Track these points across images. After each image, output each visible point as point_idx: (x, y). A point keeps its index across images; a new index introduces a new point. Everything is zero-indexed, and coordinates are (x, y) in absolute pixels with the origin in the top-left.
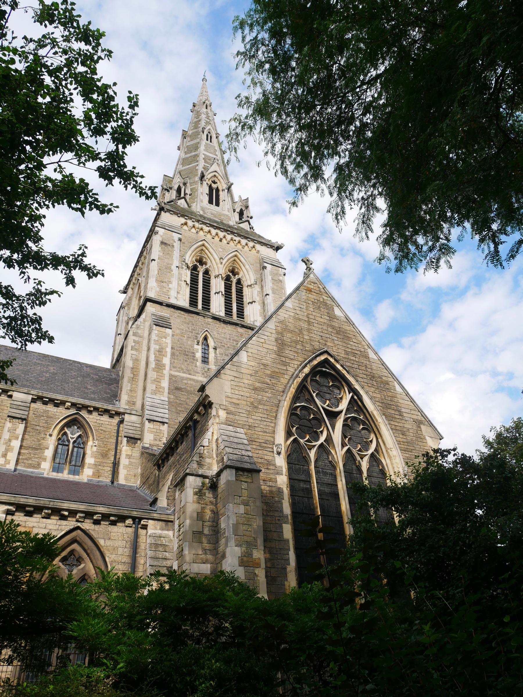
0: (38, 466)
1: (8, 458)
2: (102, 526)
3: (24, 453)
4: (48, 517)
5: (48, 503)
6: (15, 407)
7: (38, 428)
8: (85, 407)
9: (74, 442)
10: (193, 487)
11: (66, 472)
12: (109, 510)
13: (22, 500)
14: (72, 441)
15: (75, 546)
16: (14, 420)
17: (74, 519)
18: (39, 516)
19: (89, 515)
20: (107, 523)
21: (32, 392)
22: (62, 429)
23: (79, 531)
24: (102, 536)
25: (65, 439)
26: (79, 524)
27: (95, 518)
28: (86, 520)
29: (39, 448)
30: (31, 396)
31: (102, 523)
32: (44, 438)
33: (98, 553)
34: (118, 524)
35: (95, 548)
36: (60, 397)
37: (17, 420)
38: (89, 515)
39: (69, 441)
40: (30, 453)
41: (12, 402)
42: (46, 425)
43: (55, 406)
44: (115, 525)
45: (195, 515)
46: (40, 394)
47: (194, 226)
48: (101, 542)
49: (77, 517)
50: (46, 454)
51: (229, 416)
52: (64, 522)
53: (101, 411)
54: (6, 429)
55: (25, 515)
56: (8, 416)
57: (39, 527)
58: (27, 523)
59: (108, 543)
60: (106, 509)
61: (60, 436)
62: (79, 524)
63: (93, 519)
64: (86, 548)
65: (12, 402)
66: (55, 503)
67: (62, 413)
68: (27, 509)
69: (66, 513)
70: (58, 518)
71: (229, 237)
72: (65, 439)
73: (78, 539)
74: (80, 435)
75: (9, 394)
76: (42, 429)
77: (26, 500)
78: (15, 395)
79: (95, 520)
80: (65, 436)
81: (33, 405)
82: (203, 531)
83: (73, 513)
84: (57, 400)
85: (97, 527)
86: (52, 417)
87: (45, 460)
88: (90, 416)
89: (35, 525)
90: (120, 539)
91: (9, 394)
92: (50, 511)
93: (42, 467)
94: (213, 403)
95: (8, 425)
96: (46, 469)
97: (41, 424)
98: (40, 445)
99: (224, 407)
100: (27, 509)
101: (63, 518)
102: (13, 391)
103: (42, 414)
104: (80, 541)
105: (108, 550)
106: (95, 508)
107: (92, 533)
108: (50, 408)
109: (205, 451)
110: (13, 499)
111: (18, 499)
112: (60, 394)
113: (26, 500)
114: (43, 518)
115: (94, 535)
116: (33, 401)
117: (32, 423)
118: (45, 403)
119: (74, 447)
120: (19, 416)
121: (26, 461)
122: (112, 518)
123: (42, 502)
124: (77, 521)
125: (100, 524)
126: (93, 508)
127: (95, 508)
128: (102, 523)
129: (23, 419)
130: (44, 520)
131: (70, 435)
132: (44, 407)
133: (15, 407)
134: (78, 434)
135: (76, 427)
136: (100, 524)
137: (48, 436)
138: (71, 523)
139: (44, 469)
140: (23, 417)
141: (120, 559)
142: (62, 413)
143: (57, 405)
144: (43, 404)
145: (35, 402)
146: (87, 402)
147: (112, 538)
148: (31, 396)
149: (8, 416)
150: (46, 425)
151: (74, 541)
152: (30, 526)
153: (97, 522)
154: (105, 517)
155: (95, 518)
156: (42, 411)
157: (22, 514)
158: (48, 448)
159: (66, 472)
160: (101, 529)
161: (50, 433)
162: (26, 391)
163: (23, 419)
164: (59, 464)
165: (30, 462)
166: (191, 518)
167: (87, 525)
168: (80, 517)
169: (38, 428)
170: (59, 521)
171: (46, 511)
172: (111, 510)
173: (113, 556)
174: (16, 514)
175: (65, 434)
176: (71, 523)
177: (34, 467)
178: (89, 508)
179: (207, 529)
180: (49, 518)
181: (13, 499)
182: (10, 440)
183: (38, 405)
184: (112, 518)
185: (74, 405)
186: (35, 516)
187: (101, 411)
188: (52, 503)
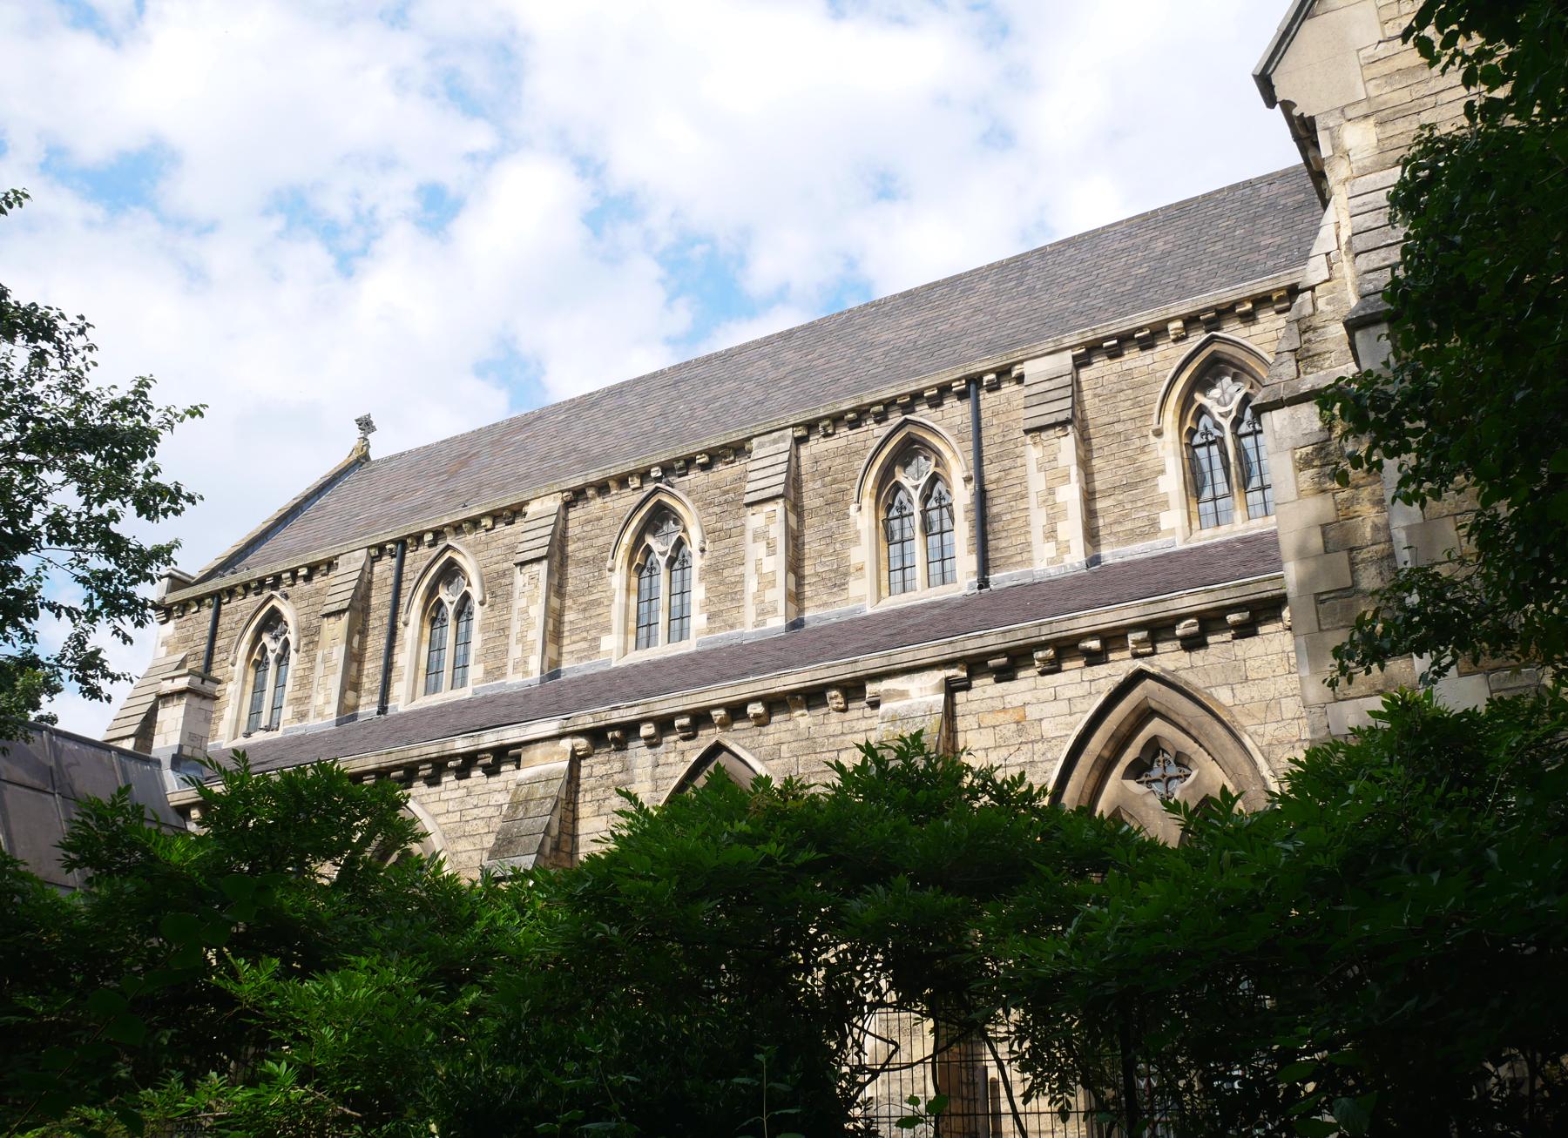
0: (1153, 527)
1: (1061, 536)
2: (1211, 649)
3: (1105, 510)
4: (1053, 667)
5: (1035, 632)
6: (1035, 400)
7: (1118, 427)
8: (1224, 313)
9: (1237, 422)
10: (1288, 444)
11: (1239, 515)
12: (1212, 597)
13: (971, 645)
14: (1226, 424)
15: (1155, 727)
16: (1044, 435)
17: (1127, 654)
18: (1032, 672)
19: (1158, 630)
20: (1228, 636)
21: (1067, 342)
22: (1187, 401)
23: (1148, 682)
24: (1220, 679)
25: (1210, 426)
26: (1140, 664)
27: (1178, 632)
28: (1160, 647)
29: (1140, 480)
30: (1069, 354)
31: (1210, 639)
32: (1142, 449)
33: (1219, 728)
34: (1261, 630)
35: (1208, 718)
36: (1144, 318)
37: (1051, 432)
38: (1158, 630)
39: (1218, 426)
40: (1121, 503)
41: (1027, 392)
42: (1135, 412)
43: (1143, 349)
44: (1255, 634)
45: (1316, 542)
46: (1090, 336)
48: (1223, 696)
49: (1131, 646)
50: (1162, 489)
51: (1390, 130)
52: (1100, 670)
53: (1280, 300)
54: (1032, 467)
55: (998, 681)
56: (1027, 432)
57: (1039, 702)
58: (1008, 699)
59: (1244, 693)
60: (1204, 598)
61: (1189, 424)
62: (1140, 664)
63: (1176, 638)
64: (1184, 724)
65: (1027, 392)
66: (1055, 627)
67: (1169, 355)
68: (991, 663)
69: (1095, 644)
70: (1081, 663)
72: (1210, 426)
73: (1153, 704)
74: (1246, 395)
75: (1014, 374)
76: (1129, 425)
77: (979, 643)
78: (1031, 369)
79: (1183, 639)
80: (1205, 420)
81: (1085, 374)
82: (1355, 583)
83: (1113, 639)
84: (1140, 329)
85: (1198, 657)
86: (1145, 384)
87: (1165, 504)
88: (1254, 329)
89: (1028, 697)
90: (1280, 671)
91: (1014, 374)
92: (1050, 653)
93: (1163, 526)
94: (1312, 119)
95: (1033, 453)
96: (1174, 528)
97: (1123, 416)
98: (1139, 470)
99: (1363, 109)
100: (991, 663)
101: (1094, 658)
102: (1021, 362)
103: (1116, 387)
104: (1163, 710)
105: (1250, 715)
106: (1170, 605)
107: (1186, 676)
108: (1134, 359)
109: (1321, 304)
110: (948, 649)
111: (959, 646)
112: (1134, 310)
113: (979, 643)
114: (1042, 673)
115: (1194, 680)
116: (1081, 362)
117: (1100, 421)
118: (1115, 353)
119: (1238, 437)
120: (1050, 420)
121: (1116, 528)
122: (1232, 618)
123: (1020, 635)
124: (1136, 656)
125: (1205, 645)
126: (1161, 607)
127: (1170, 605)
128: (1210, 639)
129: (1063, 424)
130: (1048, 678)
131: (1216, 410)
132: (1116, 365)
133: (1035, 400)
134: (1239, 397)
135: (1227, 380)
136: (1205, 645)
137: (1152, 439)
138: (1121, 666)
139: (1172, 531)
140: (1062, 417)
141: (1295, 731)
142: (1169, 355)
143: (1147, 344)
144: (1111, 357)
145: (1089, 364)
146: (1225, 295)
147: (1252, 675)
148: (1069, 354)
149: (1027, 432)
150: (1135, 412)
151: (1145, 714)
152: (1015, 704)
153: (1193, 643)
154: (1211, 621)
155: (1178, 632)
156: (1113, 378)
157: (990, 680)
158: (1162, 472)
159: (1239, 515)
160: (1212, 659)
161: (1155, 426)
162: (1050, 347)
163: (1063, 424)
164: (1215, 499)
165: (1128, 525)
166: (1302, 554)
167: (1169, 658)
168: (1135, 642)
169: (1118, 427)
170: (1088, 669)
171: (1040, 654)
172: (1218, 595)
173: (1270, 728)
174: (975, 683)
175: (1202, 411)
176: (1121, 666)
177: (1143, 535)
178: (1152, 609)
179: (1373, 571)
180: (1059, 670)
181: (948, 649)
182: (1051, 491)
183: (1101, 367)
184: (1232, 618)
185: (1191, 321)
186: (1021, 674)
187: (1280, 300)
188: (1045, 630)
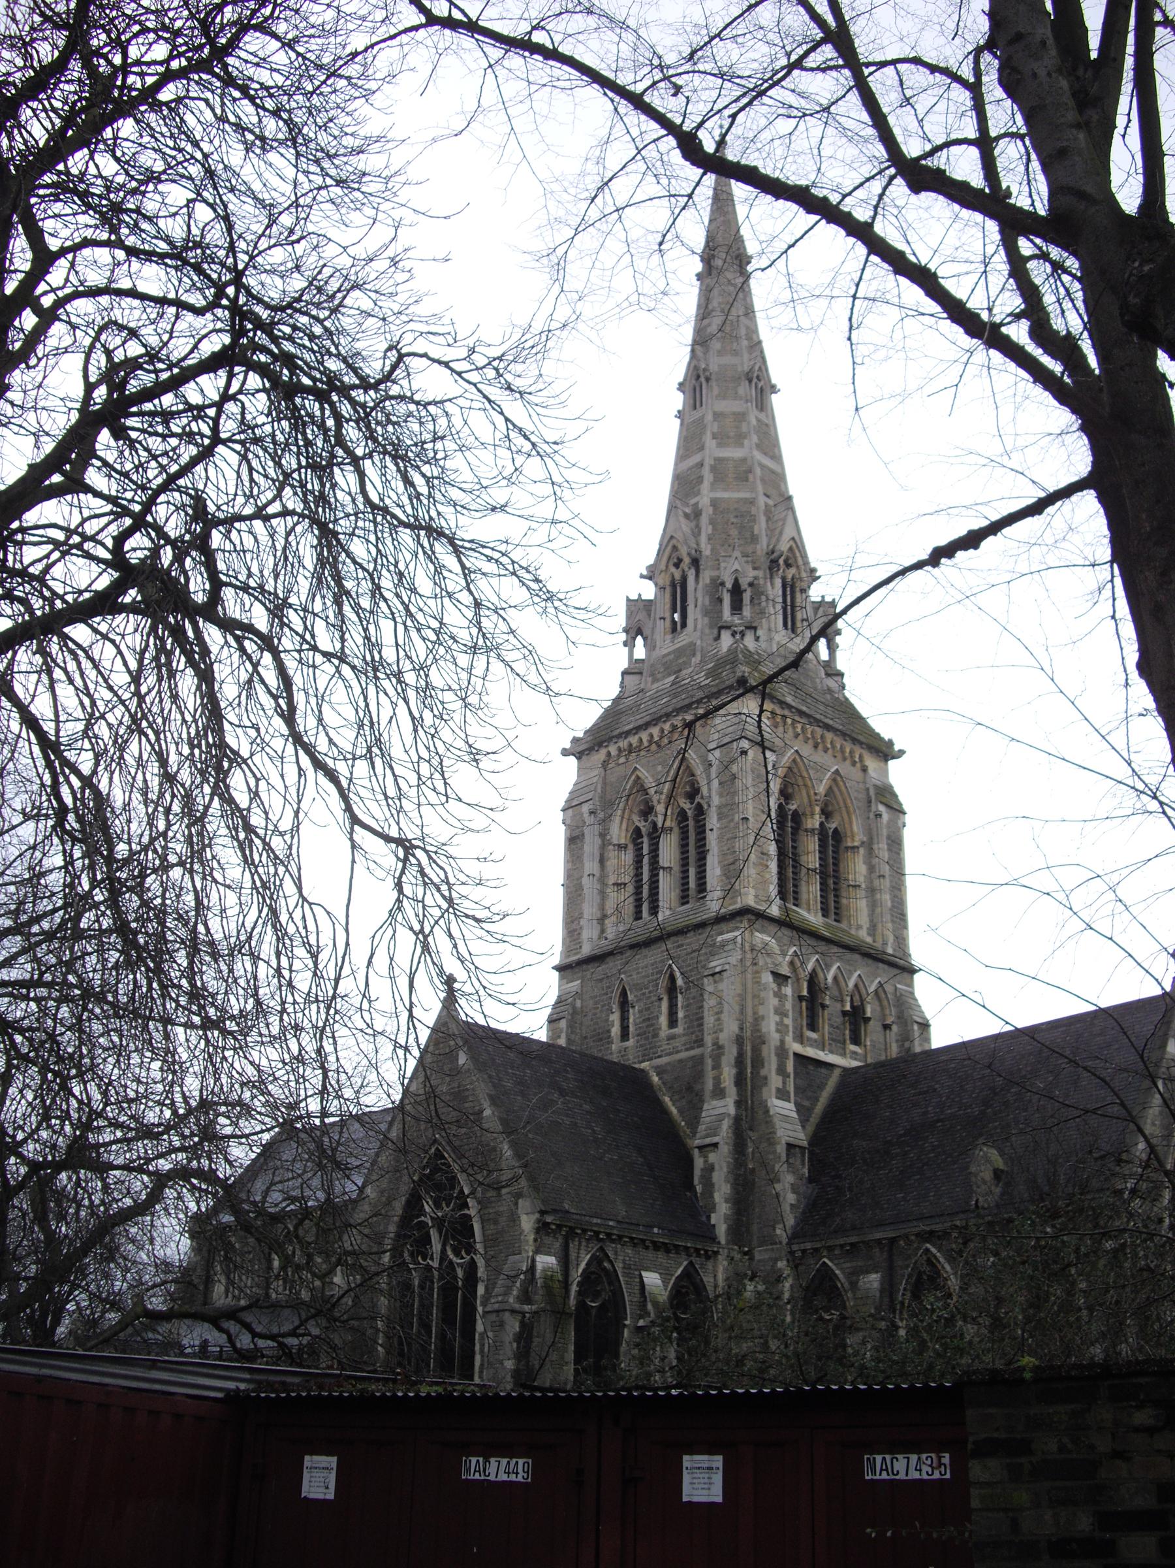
47: (620, 750)
71: (667, 727)
